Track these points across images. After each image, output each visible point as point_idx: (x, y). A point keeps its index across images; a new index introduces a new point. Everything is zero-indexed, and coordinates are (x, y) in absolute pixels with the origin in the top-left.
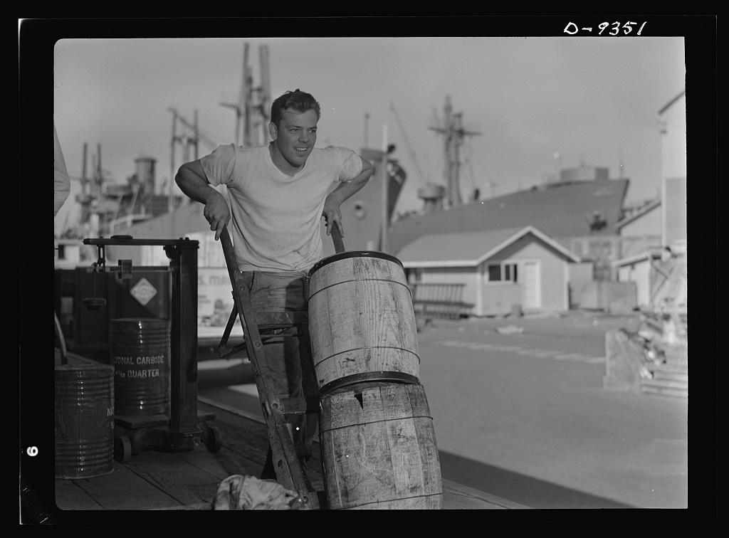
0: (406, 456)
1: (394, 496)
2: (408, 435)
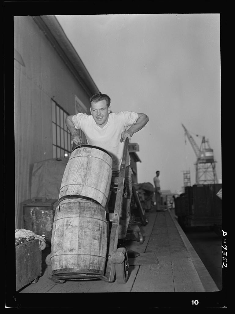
0: (70, 234)
1: (62, 253)
2: (74, 225)
